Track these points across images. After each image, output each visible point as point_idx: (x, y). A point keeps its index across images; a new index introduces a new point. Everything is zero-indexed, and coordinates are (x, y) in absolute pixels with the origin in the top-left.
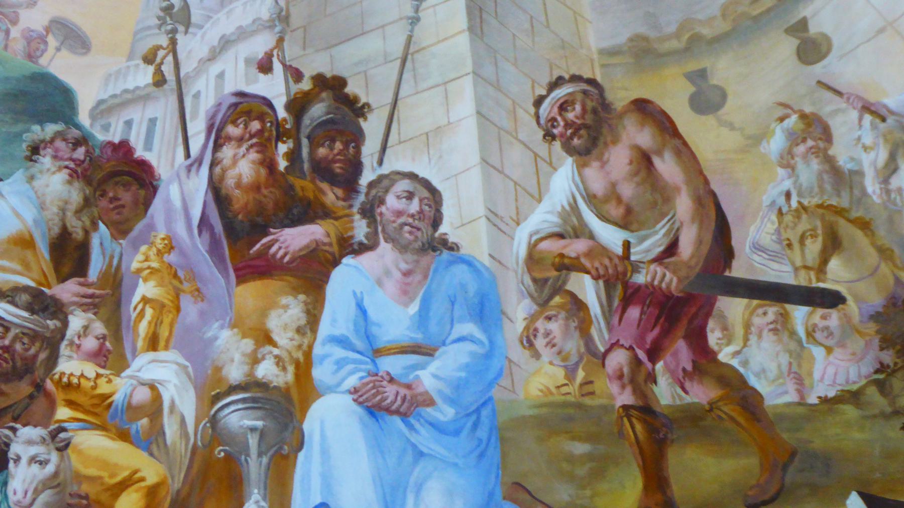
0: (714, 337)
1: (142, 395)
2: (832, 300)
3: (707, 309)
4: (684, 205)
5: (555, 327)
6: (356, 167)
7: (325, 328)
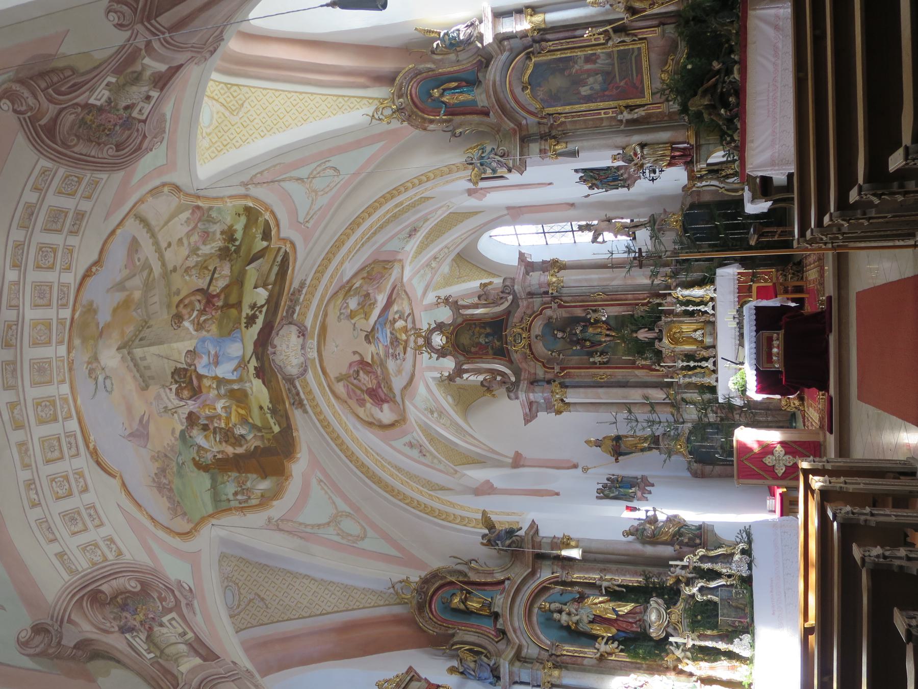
0: (215, 293)
1: (223, 410)
2: (215, 268)
3: (210, 294)
4: (193, 298)
5: (207, 326)
6: (184, 369)
7: (207, 374)
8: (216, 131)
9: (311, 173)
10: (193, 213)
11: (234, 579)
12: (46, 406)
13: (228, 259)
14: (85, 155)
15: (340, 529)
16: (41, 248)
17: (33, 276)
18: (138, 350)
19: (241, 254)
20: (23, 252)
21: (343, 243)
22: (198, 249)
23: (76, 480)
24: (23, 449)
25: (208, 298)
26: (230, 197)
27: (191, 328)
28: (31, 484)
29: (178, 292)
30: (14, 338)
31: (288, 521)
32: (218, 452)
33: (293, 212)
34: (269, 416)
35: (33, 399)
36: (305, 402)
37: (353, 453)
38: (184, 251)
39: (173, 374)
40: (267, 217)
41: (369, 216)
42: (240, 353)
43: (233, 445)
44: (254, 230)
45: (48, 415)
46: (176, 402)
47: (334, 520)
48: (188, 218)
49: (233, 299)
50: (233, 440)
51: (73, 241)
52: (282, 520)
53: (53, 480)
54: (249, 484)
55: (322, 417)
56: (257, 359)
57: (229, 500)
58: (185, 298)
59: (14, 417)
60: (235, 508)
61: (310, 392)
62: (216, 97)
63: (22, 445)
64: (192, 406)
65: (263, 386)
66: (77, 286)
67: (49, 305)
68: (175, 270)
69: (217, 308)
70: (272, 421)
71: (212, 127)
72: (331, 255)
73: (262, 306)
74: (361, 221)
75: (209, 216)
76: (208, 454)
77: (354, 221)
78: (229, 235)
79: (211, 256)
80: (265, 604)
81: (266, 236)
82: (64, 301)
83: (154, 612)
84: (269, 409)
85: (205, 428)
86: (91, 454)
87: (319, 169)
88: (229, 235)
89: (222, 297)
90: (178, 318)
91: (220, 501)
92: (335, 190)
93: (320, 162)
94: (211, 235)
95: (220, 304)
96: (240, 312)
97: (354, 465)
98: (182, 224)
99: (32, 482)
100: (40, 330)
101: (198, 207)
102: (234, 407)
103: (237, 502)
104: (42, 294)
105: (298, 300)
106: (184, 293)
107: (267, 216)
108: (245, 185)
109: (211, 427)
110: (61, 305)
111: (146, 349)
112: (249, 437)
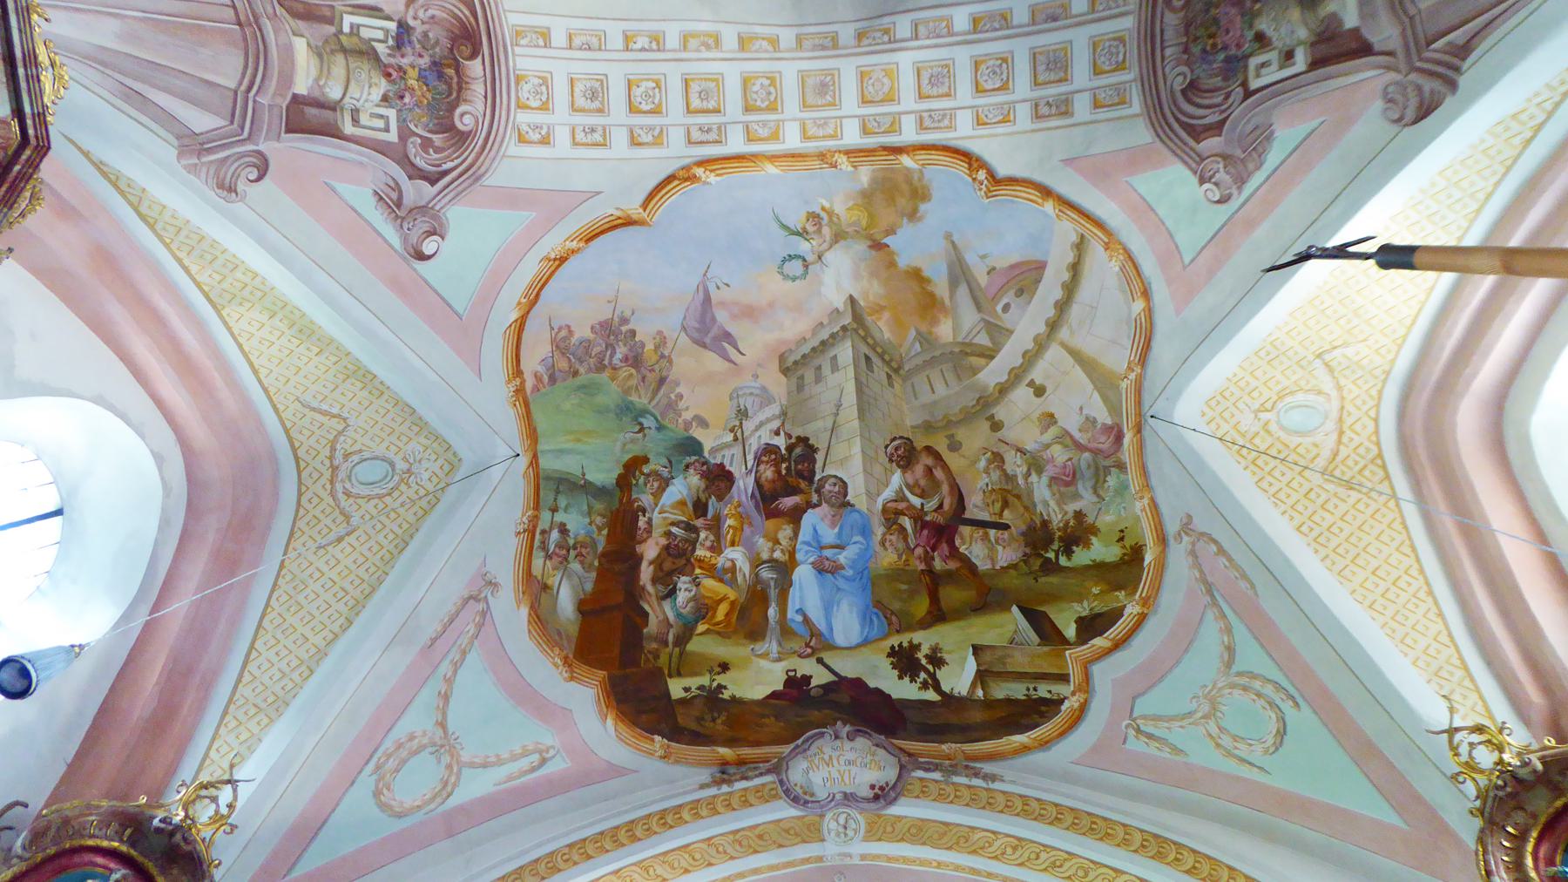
0: (958, 542)
1: (728, 564)
2: (1006, 527)
4: (945, 488)
6: (813, 473)
7: (801, 538)
8: (1280, 447)
9: (1253, 676)
10: (1107, 429)
11: (403, 487)
12: (770, 93)
13: (1028, 550)
14: (1162, 21)
15: (422, 748)
16: (1004, 60)
17: (962, 57)
18: (850, 352)
19: (1042, 580)
20: (996, 30)
21: (1105, 837)
22: (1040, 472)
23: (651, 128)
24: (711, 41)
25: (942, 532)
26: (1154, 505)
27: (888, 493)
28: (658, 44)
29: (954, 447)
30: (870, 41)
31: (480, 626)
32: (650, 522)
33: (1153, 675)
34: (704, 680)
35: (780, 72)
36: (725, 788)
37: (589, 857)
38: (1031, 438)
39: (803, 440)
40: (1128, 611)
41: (1188, 872)
42: (840, 640)
43: (657, 562)
44: (1096, 590)
45: (755, 96)
46: (754, 445)
47: (444, 743)
48: (1094, 421)
49: (952, 595)
50: (667, 566)
51: (1023, 112)
52: (484, 614)
53: (658, 83)
54: (575, 566)
55: (686, 815)
56: (827, 688)
57: (554, 510)
58: (945, 467)
59: (757, 38)
60: (536, 517)
61: (746, 803)
62: (1345, 439)
63: (715, 41)
64: (744, 484)
65: (769, 692)
66: (953, 143)
67: (921, 96)
68: (996, 426)
69: (928, 559)
70: (694, 682)
71: (1281, 434)
72: (1069, 819)
73: (937, 687)
74: (1171, 857)
75: (1107, 471)
76: (651, 497)
77: (1166, 840)
78: (1078, 533)
79: (1029, 508)
80: (328, 545)
81: (1091, 626)
82: (927, 123)
83: (410, 110)
84: (721, 687)
85: (700, 508)
86: (687, 168)
87: (1269, 690)
88: (1078, 533)
89: (952, 565)
90: (905, 455)
91: (558, 492)
92: (1231, 766)
93: (1285, 683)
94: (1072, 489)
95: (938, 564)
96: (925, 624)
97: (558, 850)
98: (1081, 409)
99: (661, 48)
100: (883, 84)
101: (1119, 438)
102: (732, 595)
103: (547, 527)
104: (936, 80)
105: (956, 774)
106: (952, 460)
107: (1132, 610)
108: (1187, 526)
109: (699, 523)
110: (921, 117)
111: (851, 369)
112: (667, 606)
